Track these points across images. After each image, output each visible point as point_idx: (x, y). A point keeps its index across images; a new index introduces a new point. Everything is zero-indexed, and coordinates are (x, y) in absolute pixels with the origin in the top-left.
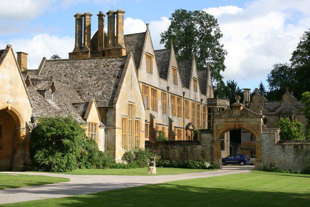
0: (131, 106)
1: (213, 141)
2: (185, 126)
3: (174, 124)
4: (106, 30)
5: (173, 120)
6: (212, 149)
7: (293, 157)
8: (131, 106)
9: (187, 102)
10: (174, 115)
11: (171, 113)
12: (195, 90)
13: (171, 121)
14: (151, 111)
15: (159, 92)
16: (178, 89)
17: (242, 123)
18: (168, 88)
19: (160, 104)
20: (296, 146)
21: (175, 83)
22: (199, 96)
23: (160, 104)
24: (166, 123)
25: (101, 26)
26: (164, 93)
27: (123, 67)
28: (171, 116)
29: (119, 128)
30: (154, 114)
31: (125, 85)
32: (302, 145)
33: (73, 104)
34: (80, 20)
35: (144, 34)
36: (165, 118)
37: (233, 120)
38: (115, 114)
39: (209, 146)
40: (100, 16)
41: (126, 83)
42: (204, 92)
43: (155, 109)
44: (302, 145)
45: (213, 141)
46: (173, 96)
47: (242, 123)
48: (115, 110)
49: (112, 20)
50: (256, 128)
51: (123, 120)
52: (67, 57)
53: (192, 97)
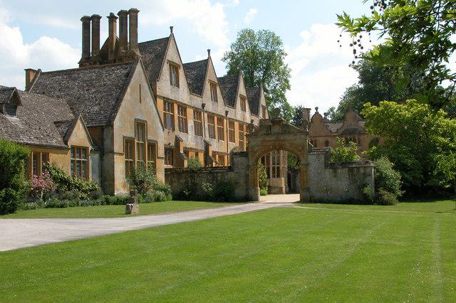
0: (141, 126)
1: (248, 166)
2: (229, 151)
3: (211, 149)
4: (117, 34)
5: (211, 143)
6: (247, 176)
7: (347, 183)
8: (141, 126)
9: (232, 123)
10: (212, 137)
11: (207, 135)
12: (244, 109)
13: (207, 145)
14: (177, 132)
15: (190, 112)
16: (220, 108)
17: (283, 143)
18: (203, 105)
19: (191, 123)
20: (85, 149)
21: (215, 99)
22: (248, 117)
23: (191, 123)
24: (201, 147)
25: (111, 30)
26: (197, 112)
27: (129, 76)
28: (208, 139)
29: (121, 154)
30: (182, 135)
31: (127, 97)
32: (358, 168)
33: (55, 123)
34: (90, 24)
35: (167, 40)
36: (199, 141)
37: (273, 138)
38: (113, 133)
39: (243, 171)
40: (112, 18)
41: (131, 95)
42: (254, 111)
43: (184, 129)
44: (358, 168)
45: (248, 166)
46: (211, 116)
47: (283, 143)
48: (113, 129)
49: (124, 21)
50: (300, 148)
51: (128, 143)
52: (77, 66)
53: (239, 117)
